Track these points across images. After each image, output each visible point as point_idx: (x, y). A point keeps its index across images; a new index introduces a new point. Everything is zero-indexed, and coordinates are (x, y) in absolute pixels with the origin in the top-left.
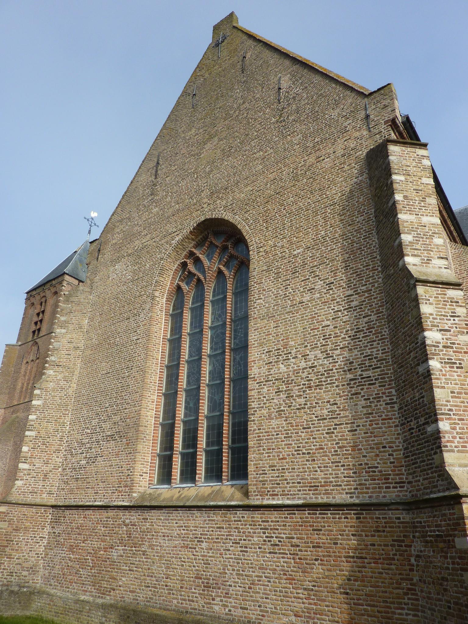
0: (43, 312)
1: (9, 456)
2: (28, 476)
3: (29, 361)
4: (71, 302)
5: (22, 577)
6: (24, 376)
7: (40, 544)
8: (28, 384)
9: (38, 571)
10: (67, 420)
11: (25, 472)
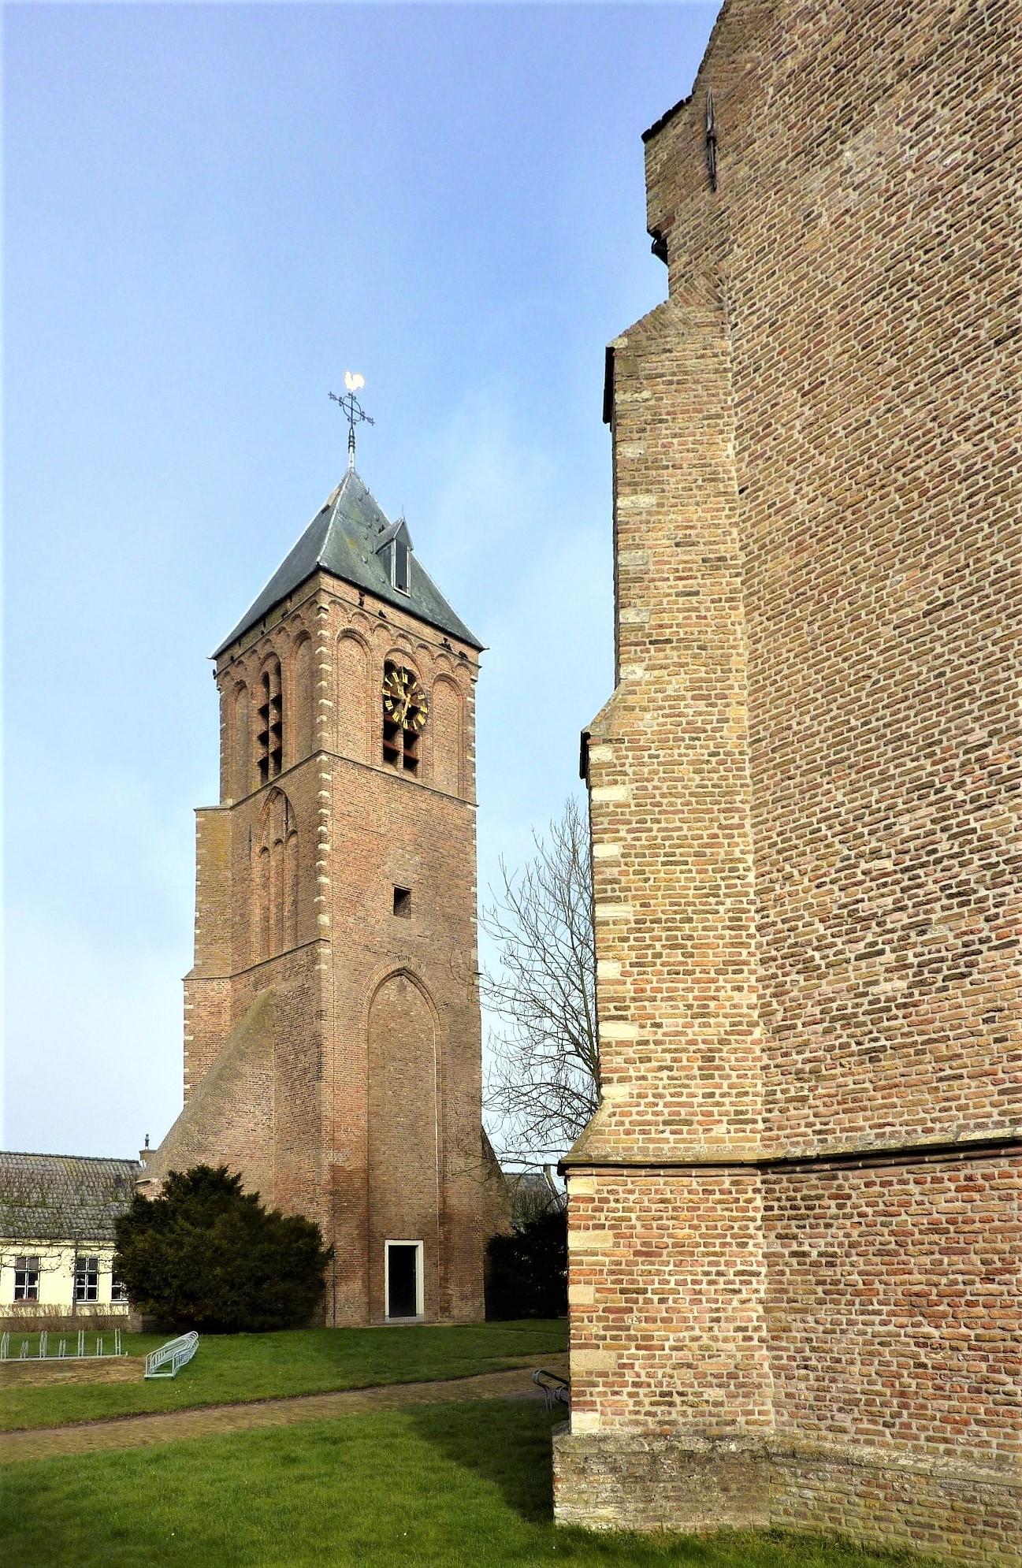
0: (278, 702)
1: (272, 1093)
2: (643, 1066)
3: (270, 846)
4: (649, 377)
5: (706, 1408)
6: (265, 886)
7: (744, 1296)
8: (280, 907)
9: (760, 1386)
10: (744, 846)
11: (630, 1052)
